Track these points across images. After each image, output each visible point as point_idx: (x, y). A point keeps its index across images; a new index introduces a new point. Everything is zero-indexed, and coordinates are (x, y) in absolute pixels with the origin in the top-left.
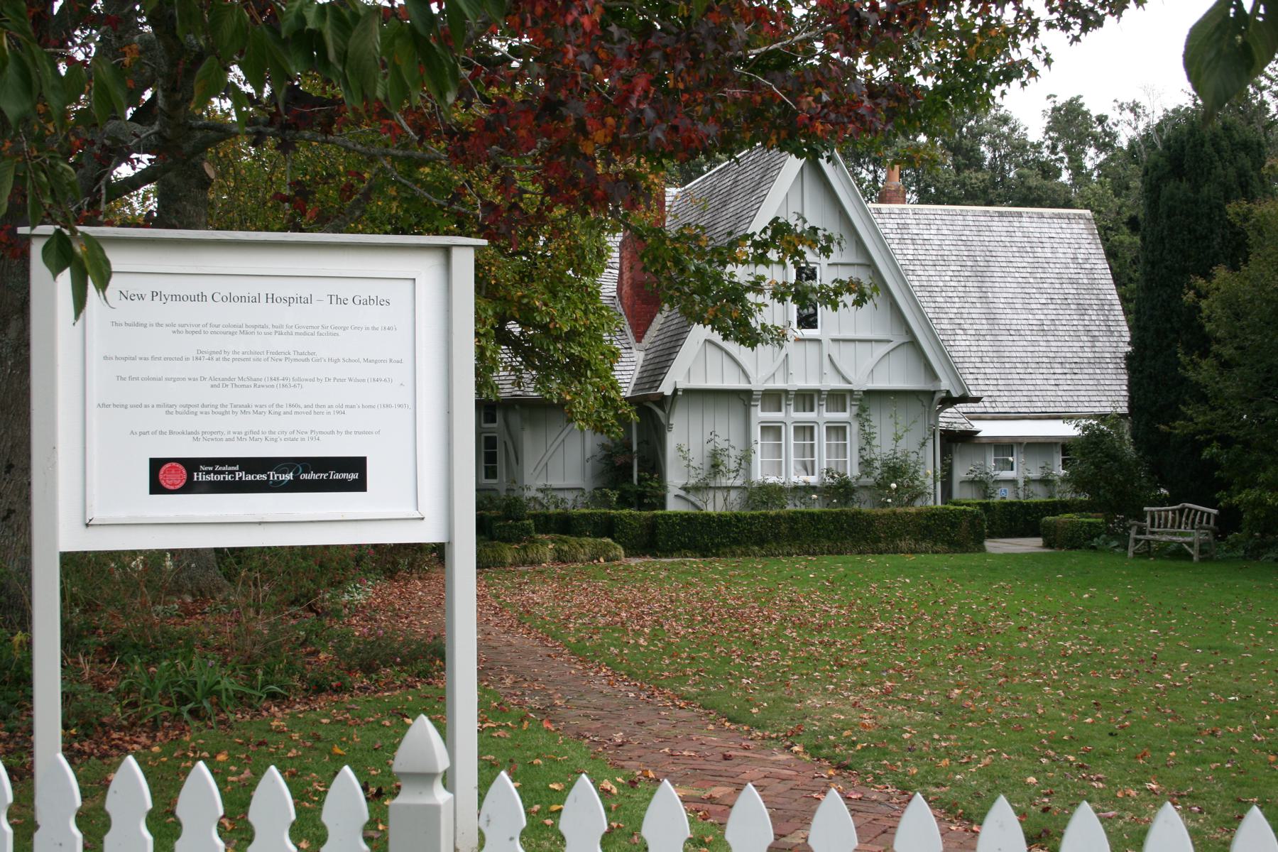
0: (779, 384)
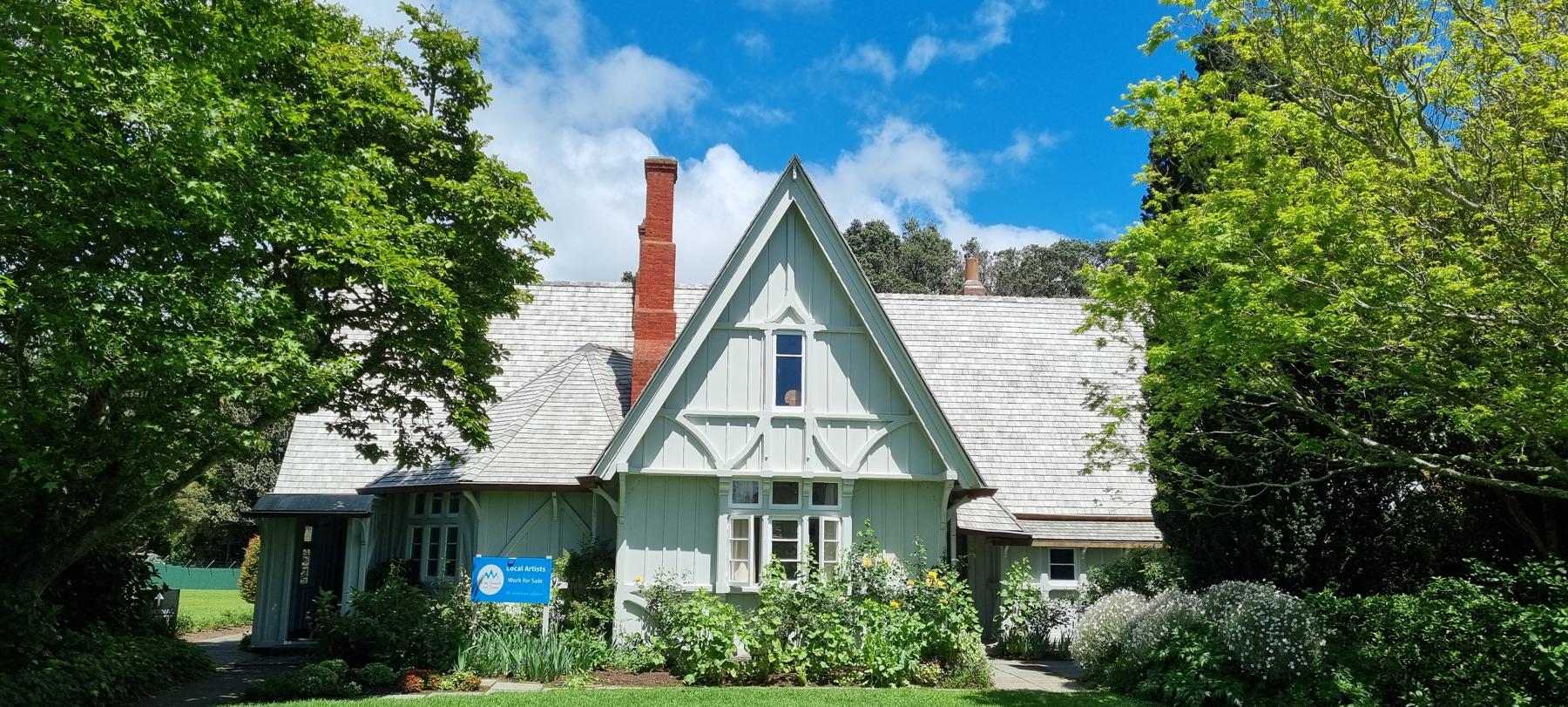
0: (752, 469)
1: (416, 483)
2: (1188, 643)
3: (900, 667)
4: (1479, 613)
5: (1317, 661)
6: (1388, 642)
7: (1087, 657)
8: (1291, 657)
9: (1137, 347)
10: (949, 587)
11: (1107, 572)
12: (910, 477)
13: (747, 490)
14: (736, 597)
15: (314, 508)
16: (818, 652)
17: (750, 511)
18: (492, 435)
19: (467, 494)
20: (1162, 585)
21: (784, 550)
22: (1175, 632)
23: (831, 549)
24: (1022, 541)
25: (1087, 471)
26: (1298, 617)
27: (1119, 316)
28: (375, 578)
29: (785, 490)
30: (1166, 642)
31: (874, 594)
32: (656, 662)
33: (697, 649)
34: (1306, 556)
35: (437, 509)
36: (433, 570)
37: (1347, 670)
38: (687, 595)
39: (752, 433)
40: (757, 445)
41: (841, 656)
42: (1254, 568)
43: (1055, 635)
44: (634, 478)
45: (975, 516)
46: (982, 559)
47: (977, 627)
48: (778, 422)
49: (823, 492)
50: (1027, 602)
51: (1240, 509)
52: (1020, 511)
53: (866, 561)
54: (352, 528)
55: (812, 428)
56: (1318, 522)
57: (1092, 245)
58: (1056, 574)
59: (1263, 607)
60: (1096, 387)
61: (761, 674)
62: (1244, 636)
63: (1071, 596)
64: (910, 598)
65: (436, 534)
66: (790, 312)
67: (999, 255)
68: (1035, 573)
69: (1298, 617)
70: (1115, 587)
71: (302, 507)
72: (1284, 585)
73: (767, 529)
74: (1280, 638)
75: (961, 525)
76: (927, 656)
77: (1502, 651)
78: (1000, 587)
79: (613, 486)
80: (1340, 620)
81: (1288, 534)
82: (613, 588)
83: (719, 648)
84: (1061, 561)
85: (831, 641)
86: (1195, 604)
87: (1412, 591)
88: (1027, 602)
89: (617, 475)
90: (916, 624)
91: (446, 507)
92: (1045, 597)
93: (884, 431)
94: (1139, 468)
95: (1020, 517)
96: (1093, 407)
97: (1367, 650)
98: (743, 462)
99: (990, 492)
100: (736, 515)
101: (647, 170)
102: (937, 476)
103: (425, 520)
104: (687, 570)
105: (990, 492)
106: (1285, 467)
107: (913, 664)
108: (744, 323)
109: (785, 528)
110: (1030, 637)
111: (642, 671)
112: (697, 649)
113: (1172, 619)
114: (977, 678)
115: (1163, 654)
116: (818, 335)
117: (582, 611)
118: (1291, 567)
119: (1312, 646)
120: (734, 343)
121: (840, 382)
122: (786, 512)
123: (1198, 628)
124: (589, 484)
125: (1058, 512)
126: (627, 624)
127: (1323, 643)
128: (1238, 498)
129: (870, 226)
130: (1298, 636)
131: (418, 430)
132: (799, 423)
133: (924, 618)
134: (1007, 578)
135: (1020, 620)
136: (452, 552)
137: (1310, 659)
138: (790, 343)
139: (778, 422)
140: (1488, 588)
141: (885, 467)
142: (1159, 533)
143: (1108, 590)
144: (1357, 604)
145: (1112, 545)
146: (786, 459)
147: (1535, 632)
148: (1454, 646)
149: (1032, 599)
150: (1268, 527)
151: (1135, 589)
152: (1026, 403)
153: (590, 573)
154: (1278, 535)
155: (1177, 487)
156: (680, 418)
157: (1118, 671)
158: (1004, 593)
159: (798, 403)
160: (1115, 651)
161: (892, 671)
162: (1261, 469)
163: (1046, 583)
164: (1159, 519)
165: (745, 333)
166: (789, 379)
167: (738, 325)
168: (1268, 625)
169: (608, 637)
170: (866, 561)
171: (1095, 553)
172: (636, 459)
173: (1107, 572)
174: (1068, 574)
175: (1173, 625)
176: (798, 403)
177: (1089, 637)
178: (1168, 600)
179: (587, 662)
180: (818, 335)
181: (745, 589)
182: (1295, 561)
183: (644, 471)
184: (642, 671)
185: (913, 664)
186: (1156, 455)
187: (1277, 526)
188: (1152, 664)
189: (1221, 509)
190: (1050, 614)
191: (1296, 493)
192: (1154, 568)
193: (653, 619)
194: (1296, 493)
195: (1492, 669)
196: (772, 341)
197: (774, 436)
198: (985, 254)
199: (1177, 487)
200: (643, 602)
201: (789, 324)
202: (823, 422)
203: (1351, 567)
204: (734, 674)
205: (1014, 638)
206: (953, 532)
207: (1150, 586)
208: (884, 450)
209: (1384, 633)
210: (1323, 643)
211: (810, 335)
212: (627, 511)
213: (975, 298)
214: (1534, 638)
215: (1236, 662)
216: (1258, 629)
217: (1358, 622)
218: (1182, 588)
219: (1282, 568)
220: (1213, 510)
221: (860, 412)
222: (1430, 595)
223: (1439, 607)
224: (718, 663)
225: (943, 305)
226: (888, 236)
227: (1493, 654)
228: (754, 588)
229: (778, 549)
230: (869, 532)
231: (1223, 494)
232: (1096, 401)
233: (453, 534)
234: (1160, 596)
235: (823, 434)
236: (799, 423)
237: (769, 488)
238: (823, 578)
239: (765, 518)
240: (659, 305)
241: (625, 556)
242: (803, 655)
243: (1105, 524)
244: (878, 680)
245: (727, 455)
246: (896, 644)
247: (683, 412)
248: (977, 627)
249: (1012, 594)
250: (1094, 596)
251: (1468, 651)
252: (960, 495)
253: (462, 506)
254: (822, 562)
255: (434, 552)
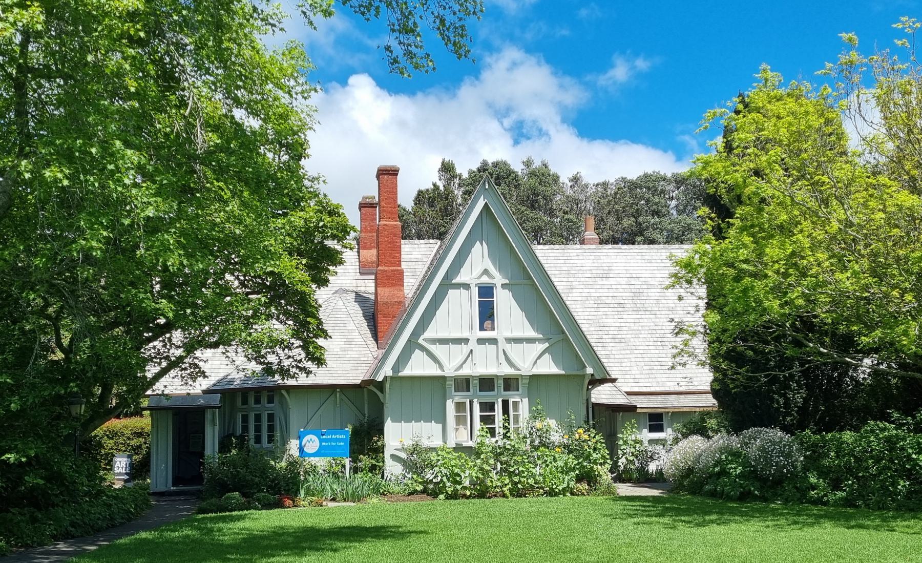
0: (466, 371)
1: (245, 386)
2: (731, 462)
3: (565, 485)
4: (888, 440)
5: (799, 468)
6: (838, 457)
7: (674, 475)
8: (784, 466)
9: (700, 298)
10: (592, 439)
11: (685, 426)
12: (563, 372)
13: (463, 384)
14: (459, 448)
15: (189, 403)
16: (516, 479)
17: (466, 397)
18: (327, 356)
19: (284, 392)
20: (716, 432)
21: (487, 420)
22: (723, 457)
23: (516, 418)
24: (631, 409)
25: (673, 368)
26: (789, 445)
27: (689, 282)
28: (224, 447)
29: (487, 383)
30: (718, 463)
31: (543, 444)
32: (418, 489)
33: (445, 479)
34: (797, 412)
35: (258, 401)
36: (258, 440)
37: (815, 473)
38: (433, 449)
39: (465, 349)
40: (469, 356)
41: (529, 481)
42: (767, 419)
43: (652, 467)
44: (396, 379)
45: (602, 395)
46: (609, 419)
47: (608, 461)
48: (481, 341)
49: (510, 383)
50: (635, 447)
51: (760, 387)
52: (628, 390)
53: (538, 425)
54: (208, 415)
55: (502, 344)
56: (804, 393)
57: (669, 175)
58: (652, 429)
59: (771, 441)
60: (678, 323)
61: (482, 492)
62: (760, 457)
63: (663, 442)
64: (566, 446)
65: (258, 418)
66: (486, 272)
67: (598, 185)
68: (639, 429)
69: (789, 445)
70: (689, 434)
71: (178, 403)
72: (785, 429)
73: (477, 407)
74: (779, 457)
75: (593, 400)
76: (579, 479)
77: (896, 459)
78: (617, 439)
79: (381, 386)
80: (814, 446)
81: (787, 399)
82: (383, 446)
83: (458, 479)
84: (656, 421)
85: (523, 472)
86: (735, 442)
87: (856, 429)
88: (635, 447)
89: (386, 377)
90: (572, 461)
91: (264, 400)
92: (646, 443)
93: (547, 345)
94: (703, 364)
95: (629, 394)
96: (677, 334)
97: (826, 462)
98: (461, 366)
99: (613, 381)
100: (457, 400)
101: (378, 177)
102: (580, 369)
103: (254, 409)
104: (428, 434)
105: (613, 381)
106: (785, 363)
107: (572, 484)
108: (457, 280)
109: (488, 407)
110: (638, 469)
111: (410, 494)
112: (445, 479)
113: (721, 450)
114: (609, 491)
115: (716, 469)
116: (504, 286)
117: (365, 461)
118: (789, 419)
119: (796, 460)
120: (451, 292)
121: (518, 315)
122: (487, 397)
123: (736, 454)
124: (366, 383)
125: (653, 390)
126: (393, 469)
127: (802, 459)
128: (759, 380)
129: (496, 165)
130: (788, 456)
131: (289, 357)
132: (494, 341)
133: (577, 458)
134: (623, 433)
135: (631, 458)
136: (271, 429)
137: (795, 467)
138: (486, 292)
139: (481, 341)
140: (899, 426)
141: (547, 366)
142: (715, 402)
143: (685, 436)
144: (823, 437)
145: (688, 410)
146: (486, 364)
147: (912, 448)
148: (872, 457)
149: (638, 445)
150: (776, 396)
151: (702, 435)
152: (629, 318)
153: (366, 440)
154: (782, 401)
155: (725, 375)
156: (421, 341)
157: (692, 482)
158: (621, 442)
159: (493, 329)
160: (690, 471)
161: (560, 488)
162: (772, 363)
163: (646, 435)
164: (715, 393)
165: (459, 286)
166: (487, 314)
167: (454, 281)
168: (773, 450)
169: (383, 477)
170: (538, 425)
171: (677, 415)
172: (396, 368)
173: (685, 426)
174: (660, 429)
175: (722, 453)
176: (493, 329)
177: (675, 464)
178: (720, 440)
179: (377, 491)
180: (504, 286)
181: (465, 444)
182: (791, 415)
183: (400, 374)
184: (410, 494)
185: (572, 484)
186: (713, 357)
187: (781, 395)
188: (711, 476)
189: (750, 387)
190: (649, 454)
191: (792, 376)
192: (712, 423)
193: (409, 466)
194: (792, 376)
195: (890, 469)
196: (475, 291)
197: (479, 350)
198: (587, 186)
199: (725, 375)
200: (403, 455)
201: (485, 279)
202: (509, 340)
203: (822, 418)
204: (468, 493)
205: (626, 470)
206: (590, 406)
207: (711, 434)
208: (547, 356)
209: (836, 453)
210: (802, 459)
211: (499, 286)
212: (390, 400)
213: (593, 246)
214: (910, 451)
215: (755, 471)
216: (767, 453)
217: (824, 447)
218: (728, 432)
219: (784, 420)
220: (745, 388)
221: (531, 333)
222: (866, 432)
223: (865, 437)
224: (459, 487)
225: (573, 250)
226: (510, 172)
227: (891, 461)
228: (470, 444)
229: (484, 419)
230: (539, 407)
231: (749, 379)
232: (679, 330)
233: (271, 417)
234: (716, 438)
235: (509, 348)
236: (494, 341)
237: (477, 382)
238: (512, 435)
239: (475, 400)
240: (392, 264)
241: (390, 427)
242: (507, 481)
243: (682, 396)
244: (551, 493)
245: (452, 362)
246: (562, 473)
247: (422, 337)
248: (608, 461)
249: (626, 442)
250: (676, 441)
251: (878, 460)
252: (595, 382)
253: (276, 399)
254: (512, 426)
255: (258, 429)
